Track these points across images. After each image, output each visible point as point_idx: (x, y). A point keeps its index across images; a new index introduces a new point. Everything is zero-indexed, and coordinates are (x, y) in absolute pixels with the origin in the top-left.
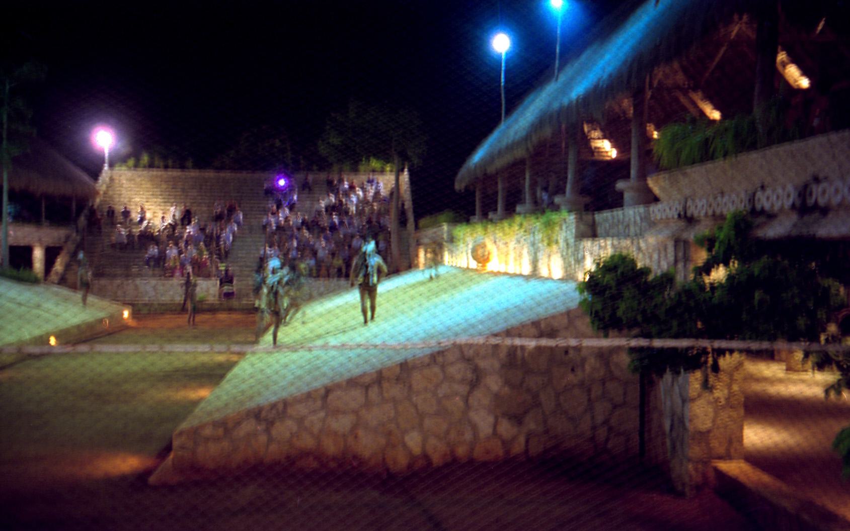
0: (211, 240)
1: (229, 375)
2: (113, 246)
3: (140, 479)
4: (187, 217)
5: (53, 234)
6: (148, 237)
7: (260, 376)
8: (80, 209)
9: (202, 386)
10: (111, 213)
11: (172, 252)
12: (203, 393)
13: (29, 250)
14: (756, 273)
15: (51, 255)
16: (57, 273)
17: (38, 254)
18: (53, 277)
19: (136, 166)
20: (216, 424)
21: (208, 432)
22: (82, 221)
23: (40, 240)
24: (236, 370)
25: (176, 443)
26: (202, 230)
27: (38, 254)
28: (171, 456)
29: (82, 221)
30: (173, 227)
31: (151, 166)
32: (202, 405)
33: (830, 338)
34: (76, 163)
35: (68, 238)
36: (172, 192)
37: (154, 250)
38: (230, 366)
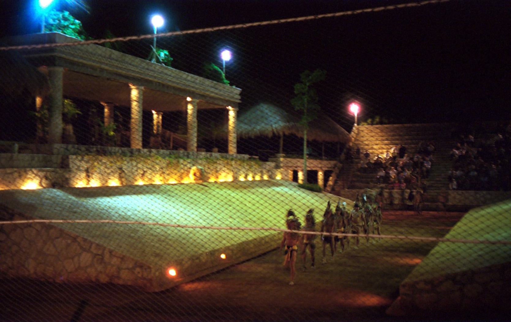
0: (416, 165)
1: (433, 251)
2: (359, 170)
3: (380, 310)
4: (401, 152)
5: (327, 164)
6: (378, 164)
7: (453, 253)
8: (341, 150)
9: (416, 257)
10: (358, 151)
11: (393, 173)
12: (417, 261)
13: (315, 173)
14: (391, 156)
15: (327, 175)
16: (330, 185)
17: (320, 175)
18: (329, 189)
19: (372, 124)
20: (426, 282)
21: (421, 286)
22: (343, 156)
23: (321, 168)
24: (437, 248)
25: (402, 290)
26: (412, 159)
27: (320, 175)
28: (399, 298)
29: (343, 156)
30: (394, 158)
31: (381, 123)
32: (417, 268)
33: (420, 165)
34: (338, 122)
35: (335, 165)
36: (392, 140)
37: (382, 173)
38: (434, 244)
